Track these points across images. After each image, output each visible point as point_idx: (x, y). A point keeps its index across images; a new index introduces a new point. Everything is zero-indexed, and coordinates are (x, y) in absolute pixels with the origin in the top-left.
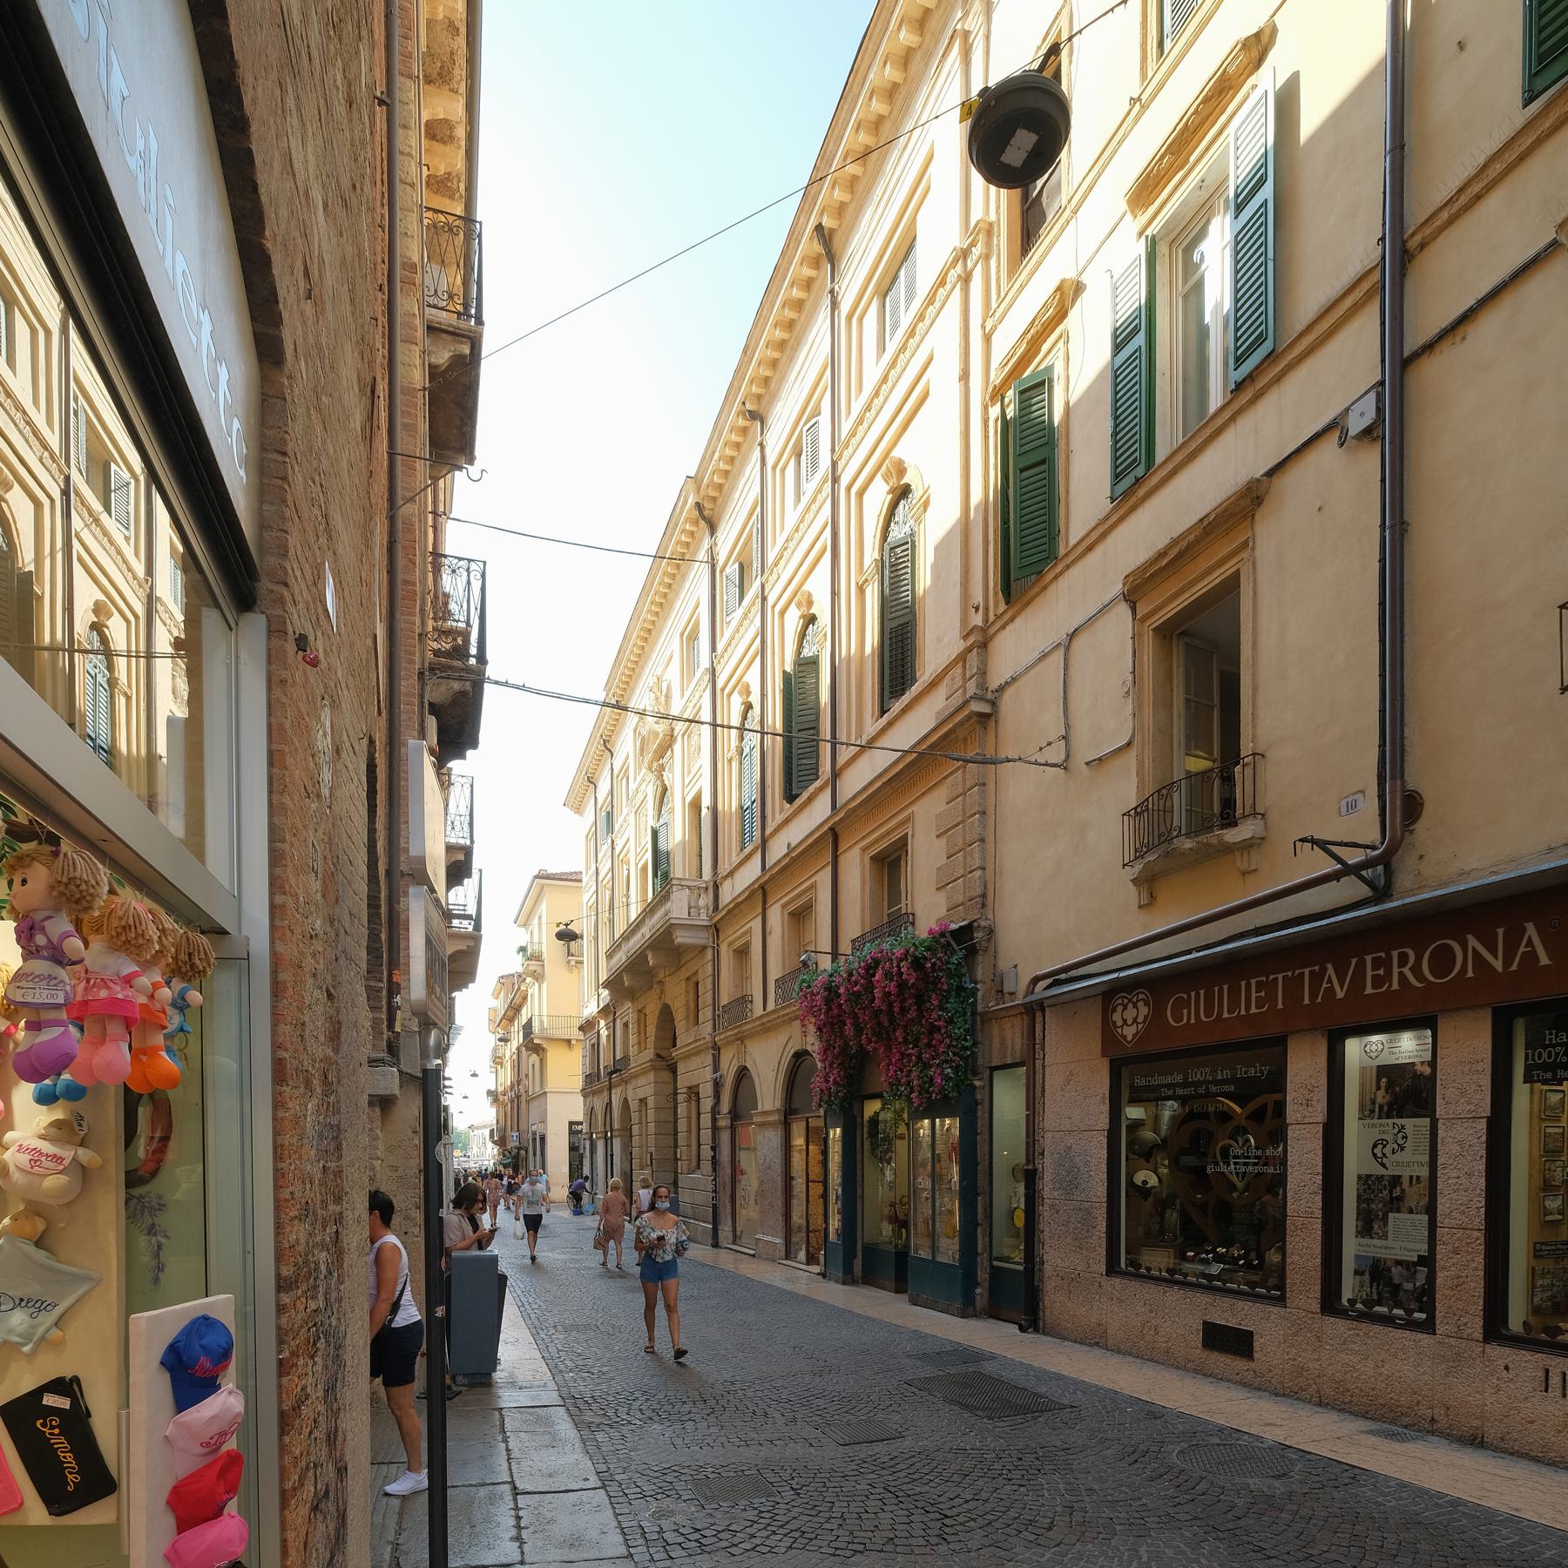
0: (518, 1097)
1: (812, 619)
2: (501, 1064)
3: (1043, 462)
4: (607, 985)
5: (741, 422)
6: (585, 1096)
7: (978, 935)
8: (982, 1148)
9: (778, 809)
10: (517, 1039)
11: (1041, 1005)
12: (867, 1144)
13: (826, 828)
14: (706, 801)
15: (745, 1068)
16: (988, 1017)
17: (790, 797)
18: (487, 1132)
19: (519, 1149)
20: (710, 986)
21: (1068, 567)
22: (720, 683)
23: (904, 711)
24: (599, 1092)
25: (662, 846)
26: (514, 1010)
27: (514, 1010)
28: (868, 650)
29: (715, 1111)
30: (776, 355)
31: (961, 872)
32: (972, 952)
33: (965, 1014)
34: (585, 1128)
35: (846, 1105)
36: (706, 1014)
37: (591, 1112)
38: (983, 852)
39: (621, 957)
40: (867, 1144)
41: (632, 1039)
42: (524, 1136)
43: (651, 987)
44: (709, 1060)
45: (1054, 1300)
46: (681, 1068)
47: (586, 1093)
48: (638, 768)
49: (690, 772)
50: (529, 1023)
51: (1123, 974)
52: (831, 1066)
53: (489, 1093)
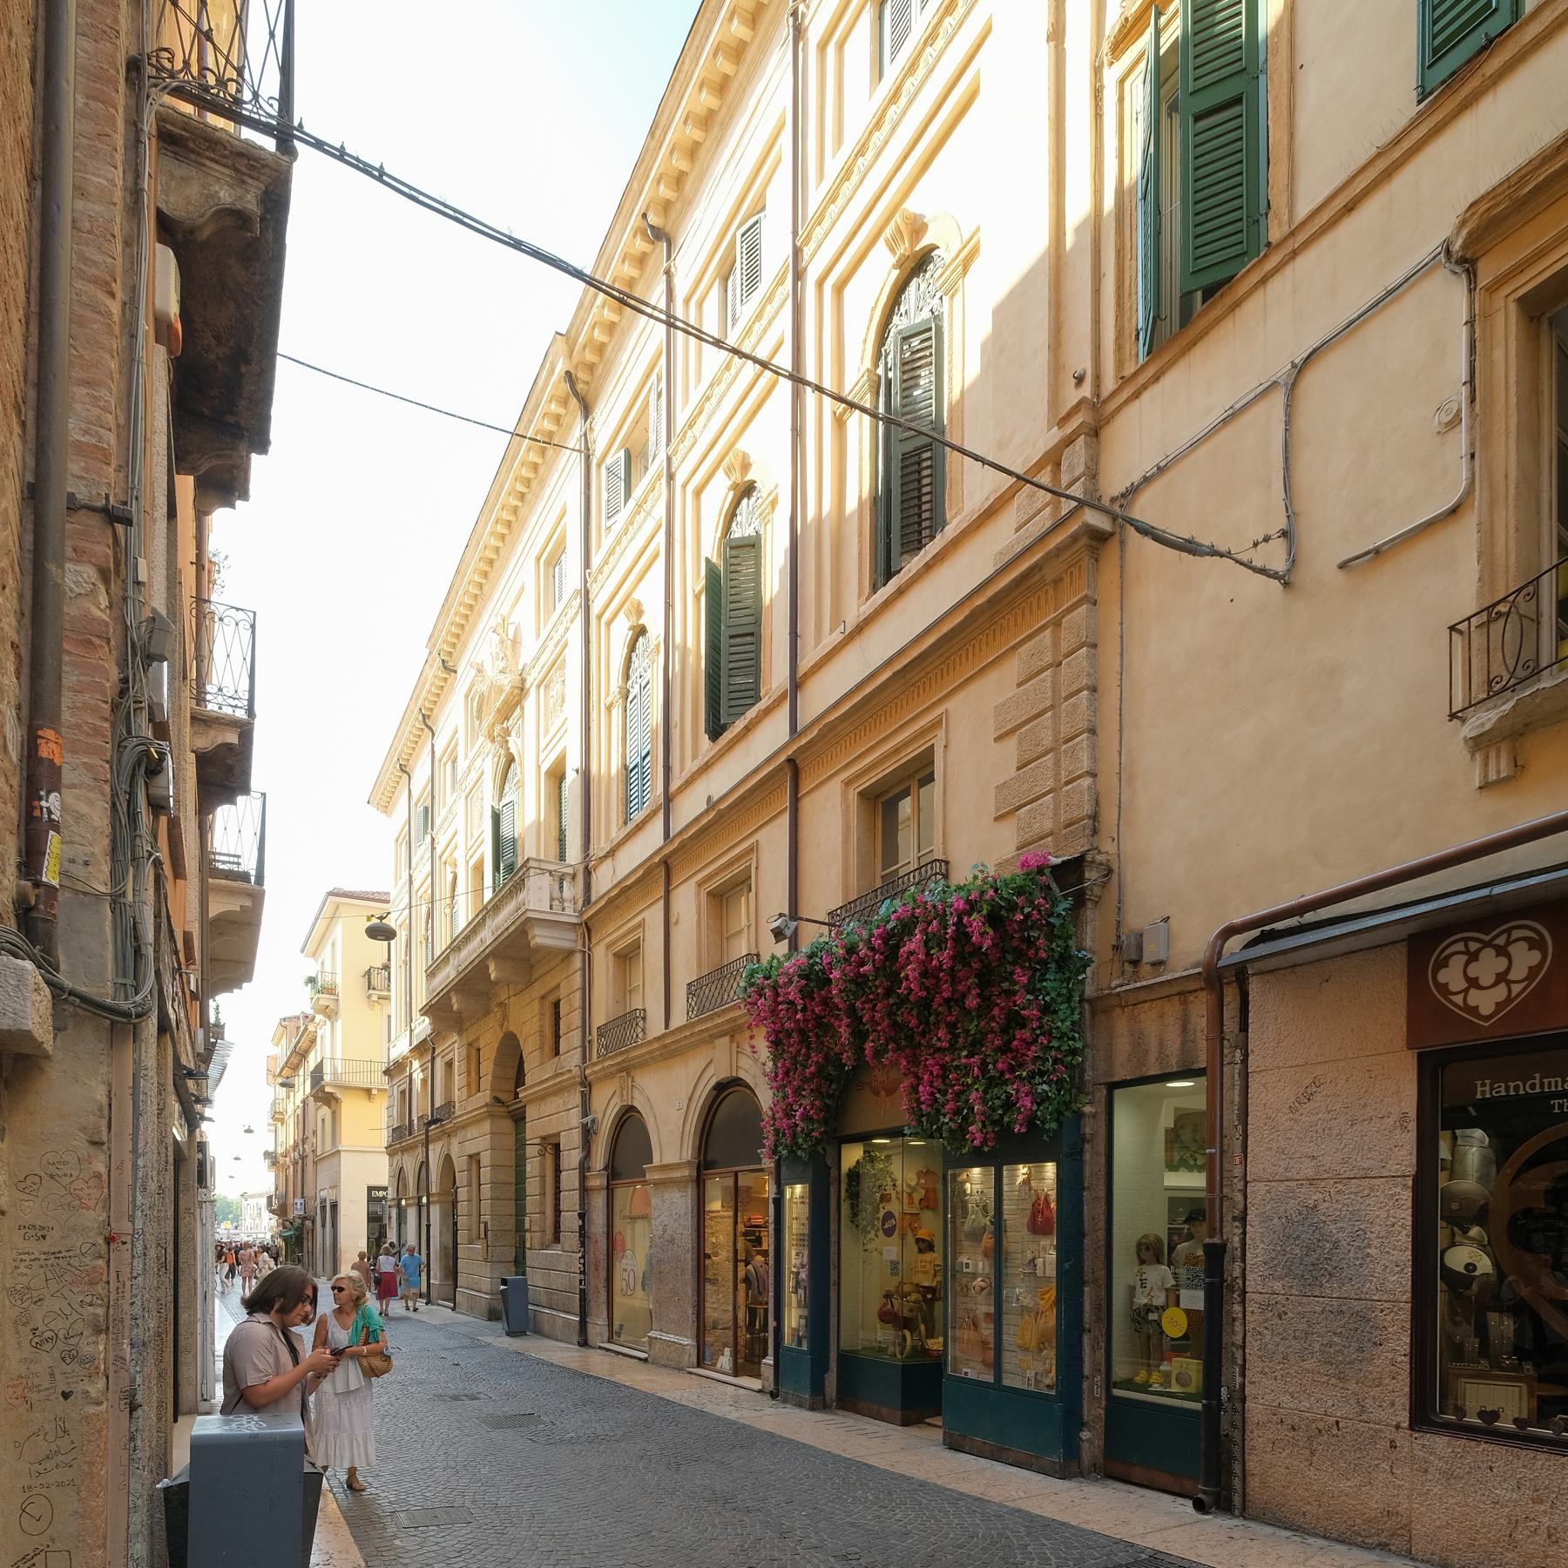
0: (303, 1158)
1: (641, 631)
2: (282, 1121)
3: (1237, 101)
4: (428, 1010)
5: (640, 245)
6: (391, 1155)
7: (1091, 875)
8: (1092, 1211)
9: (693, 743)
10: (303, 1087)
11: (1240, 973)
12: (845, 1206)
13: (783, 758)
14: (573, 762)
15: (632, 1109)
16: (1102, 1006)
17: (715, 731)
18: (263, 1202)
19: (304, 1219)
20: (577, 1003)
21: (1294, 254)
22: (595, 609)
23: (928, 567)
24: (412, 1148)
25: (506, 831)
26: (300, 1055)
27: (300, 1055)
28: (851, 505)
29: (584, 1167)
30: (697, 135)
31: (1050, 784)
32: (1080, 900)
33: (1069, 1000)
34: (391, 1194)
35: (814, 1152)
36: (571, 1040)
37: (399, 1175)
38: (1093, 747)
39: (449, 973)
40: (845, 1206)
41: (458, 1079)
42: (311, 1204)
43: (487, 1013)
44: (575, 1099)
45: (1267, 1461)
46: (531, 1113)
47: (392, 1151)
48: (472, 737)
49: (549, 733)
50: (319, 1068)
51: (1498, 890)
52: (797, 1092)
53: (267, 1154)
